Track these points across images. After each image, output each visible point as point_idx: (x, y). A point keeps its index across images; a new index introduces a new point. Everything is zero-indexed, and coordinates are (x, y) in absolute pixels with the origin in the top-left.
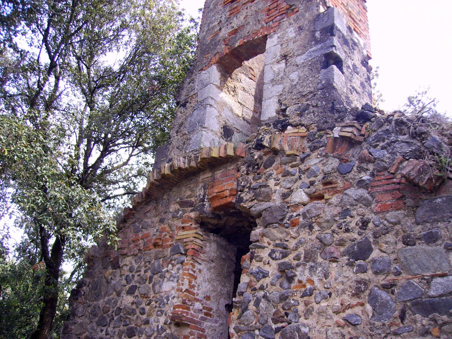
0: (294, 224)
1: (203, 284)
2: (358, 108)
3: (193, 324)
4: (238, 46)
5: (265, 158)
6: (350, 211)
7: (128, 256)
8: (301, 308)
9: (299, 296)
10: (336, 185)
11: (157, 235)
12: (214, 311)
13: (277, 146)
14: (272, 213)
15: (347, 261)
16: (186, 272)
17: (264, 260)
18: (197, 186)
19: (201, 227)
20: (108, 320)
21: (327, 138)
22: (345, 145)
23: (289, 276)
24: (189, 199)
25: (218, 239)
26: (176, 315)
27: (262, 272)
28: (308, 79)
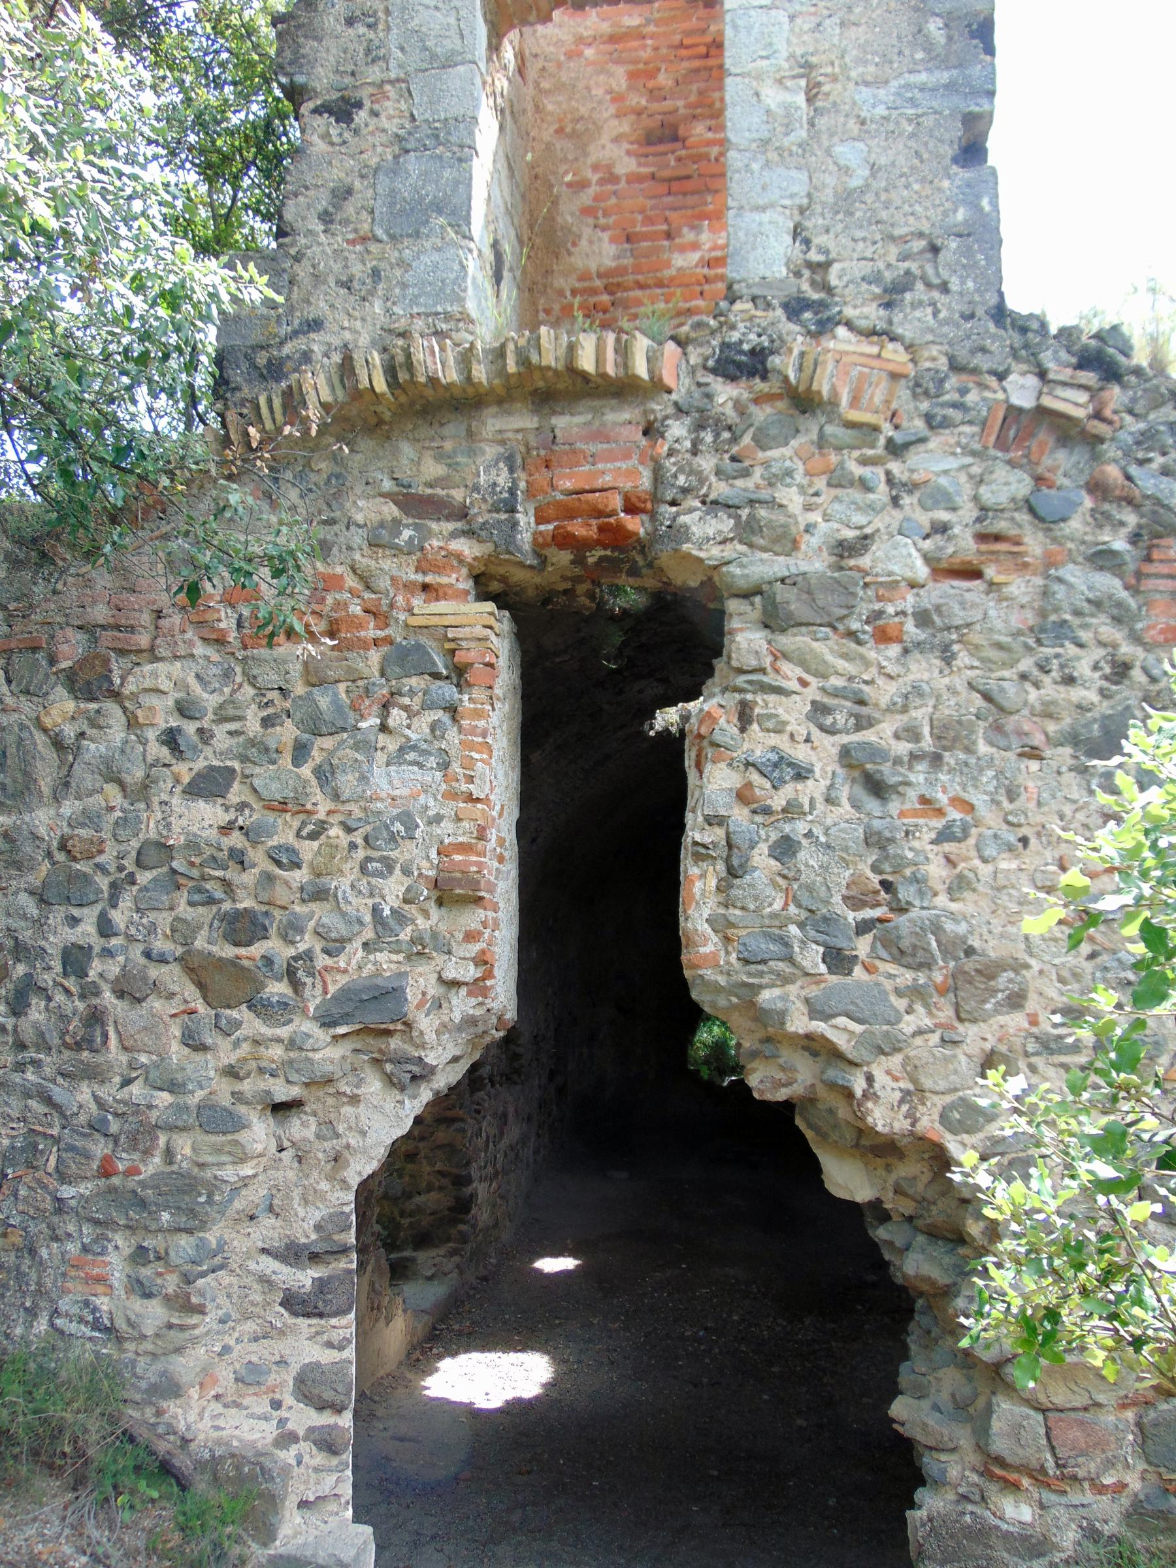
0: (883, 637)
8: (936, 871)
15: (1071, 762)
17: (789, 728)
22: (1044, 435)
24: (439, 491)
26: (458, 875)
27: (790, 764)
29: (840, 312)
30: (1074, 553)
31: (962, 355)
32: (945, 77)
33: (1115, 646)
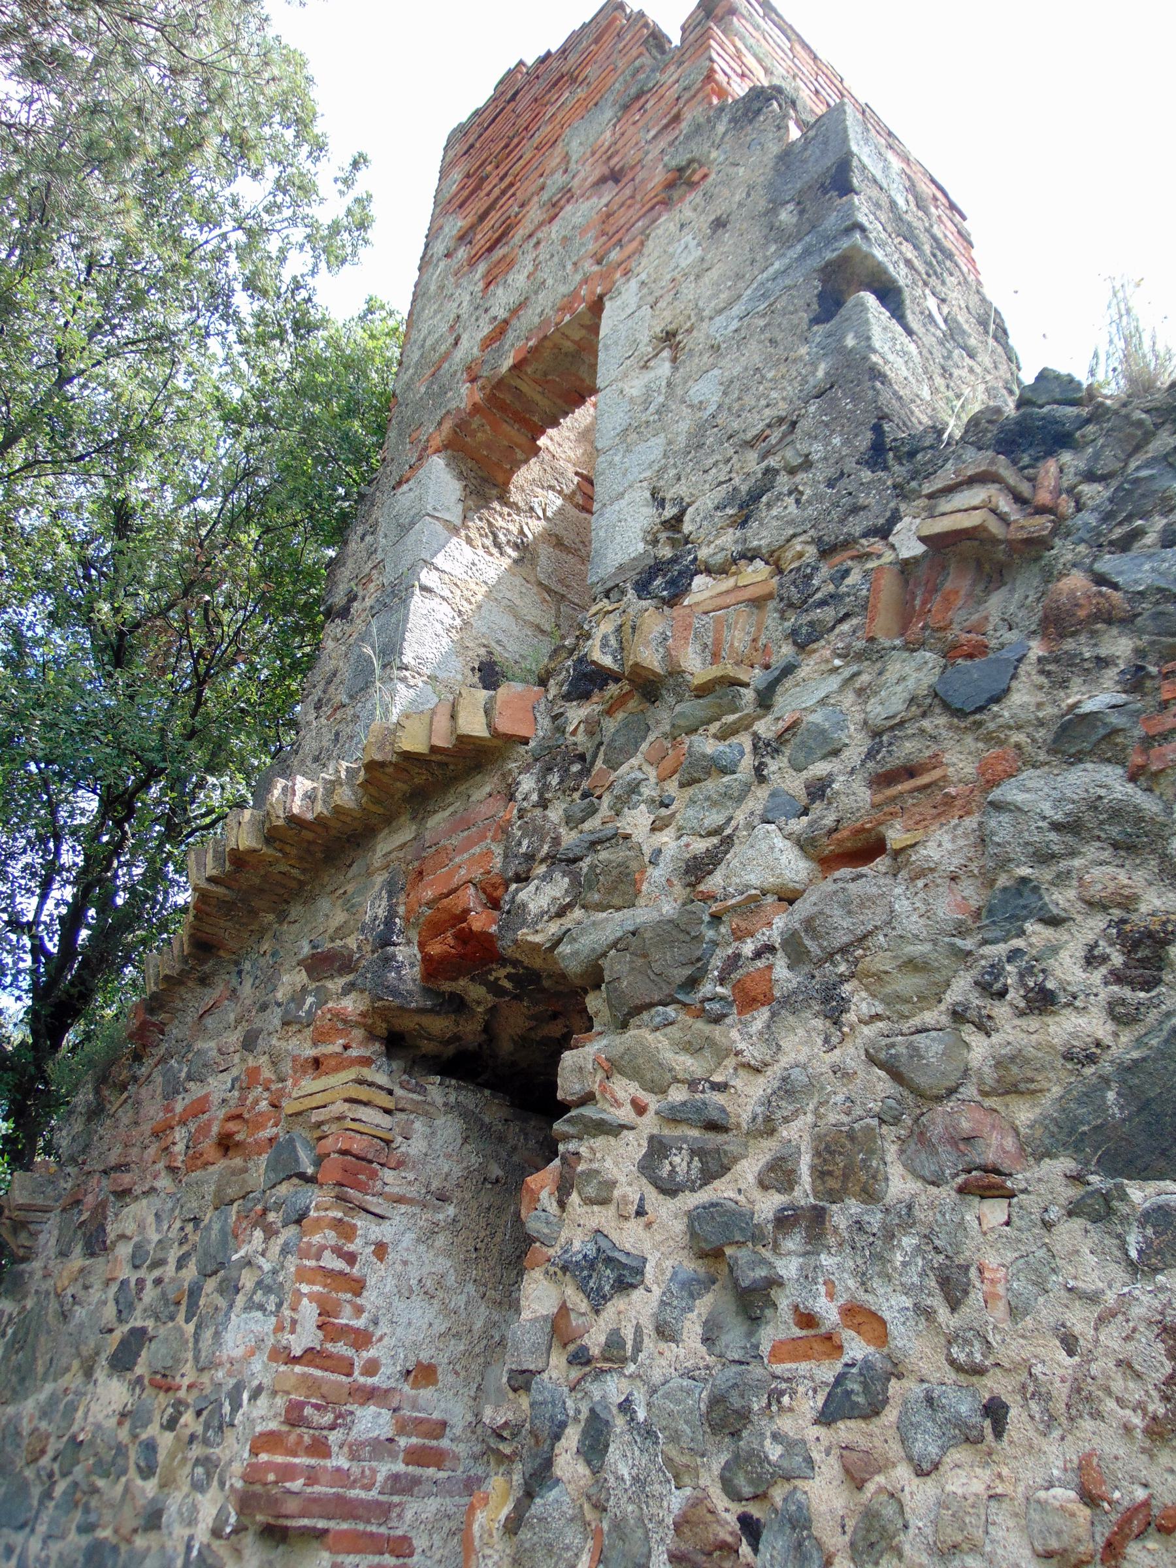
0: (748, 1001)
1: (399, 1305)
2: (998, 411)
3: (345, 1526)
4: (510, 369)
5: (611, 725)
6: (1036, 889)
7: (137, 1198)
9: (811, 1415)
10: (936, 774)
11: (232, 1103)
12: (458, 1431)
13: (651, 658)
14: (645, 956)
15: (1073, 1192)
16: (307, 1262)
18: (362, 891)
19: (390, 1055)
20: (36, 1491)
21: (866, 573)
22: (958, 583)
23: (745, 1283)
25: (469, 1098)
27: (609, 1261)
28: (763, 377)
29: (695, 559)
30: (1029, 749)
31: (832, 532)
32: (799, 248)
33: (1128, 902)
